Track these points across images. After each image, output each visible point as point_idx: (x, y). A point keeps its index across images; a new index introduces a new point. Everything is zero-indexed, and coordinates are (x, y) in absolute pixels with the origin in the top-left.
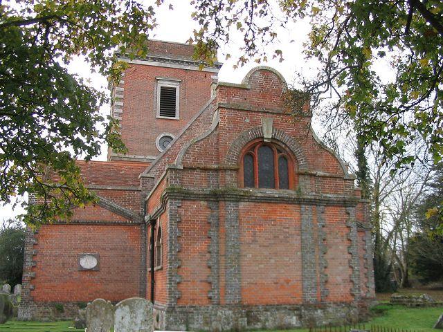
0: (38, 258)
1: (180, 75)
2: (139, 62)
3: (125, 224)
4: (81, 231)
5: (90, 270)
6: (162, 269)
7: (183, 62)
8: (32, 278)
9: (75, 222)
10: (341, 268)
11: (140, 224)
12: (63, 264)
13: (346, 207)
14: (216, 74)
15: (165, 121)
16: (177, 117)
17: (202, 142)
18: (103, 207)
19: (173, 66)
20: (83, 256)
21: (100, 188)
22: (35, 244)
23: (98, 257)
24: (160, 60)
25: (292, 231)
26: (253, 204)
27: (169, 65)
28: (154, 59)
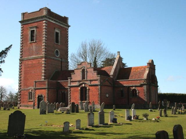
2: (51, 21)
14: (68, 29)
24: (56, 21)
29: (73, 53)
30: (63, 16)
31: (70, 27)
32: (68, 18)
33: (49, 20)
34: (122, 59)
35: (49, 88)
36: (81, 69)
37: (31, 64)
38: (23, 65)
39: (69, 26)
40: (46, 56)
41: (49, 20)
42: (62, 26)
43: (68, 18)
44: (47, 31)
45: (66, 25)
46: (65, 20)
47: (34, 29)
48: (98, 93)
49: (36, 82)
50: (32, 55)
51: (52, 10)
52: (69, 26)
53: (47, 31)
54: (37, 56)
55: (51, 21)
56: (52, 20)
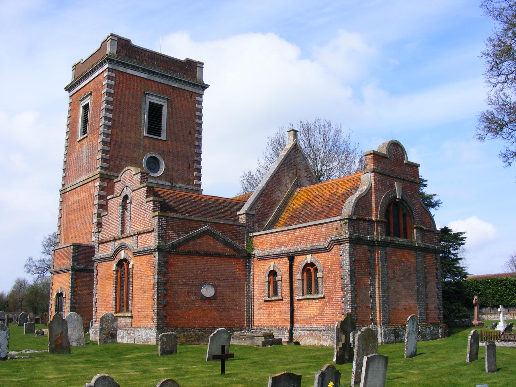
0: (168, 287)
1: (164, 91)
2: (129, 71)
3: (234, 257)
4: (201, 261)
5: (209, 299)
6: (324, 298)
7: (171, 78)
8: (165, 305)
9: (185, 252)
10: (433, 299)
11: (245, 257)
12: (188, 292)
13: (435, 254)
14: (201, 96)
15: (152, 140)
16: (163, 137)
17: (363, 198)
18: (217, 240)
19: (162, 81)
20: (202, 285)
21: (215, 221)
22: (165, 273)
23: (215, 286)
24: (149, 72)
25: (412, 270)
26: (392, 249)
27: (158, 79)
28: (144, 71)
29: (466, 241)
30: (182, 58)
31: (206, 92)
32: (203, 64)
33: (122, 69)
34: (463, 236)
35: (81, 270)
36: (120, 196)
37: (79, 201)
38: (65, 206)
39: (204, 87)
40: (104, 172)
41: (122, 69)
42: (176, 85)
43: (203, 64)
44: (142, 104)
45: (189, 83)
46: (190, 69)
47: (148, 104)
48: (153, 281)
49: (54, 250)
50: (81, 175)
51: (136, 42)
52: (204, 87)
53: (142, 104)
54: (377, 279)
55: (129, 71)
56: (134, 68)
